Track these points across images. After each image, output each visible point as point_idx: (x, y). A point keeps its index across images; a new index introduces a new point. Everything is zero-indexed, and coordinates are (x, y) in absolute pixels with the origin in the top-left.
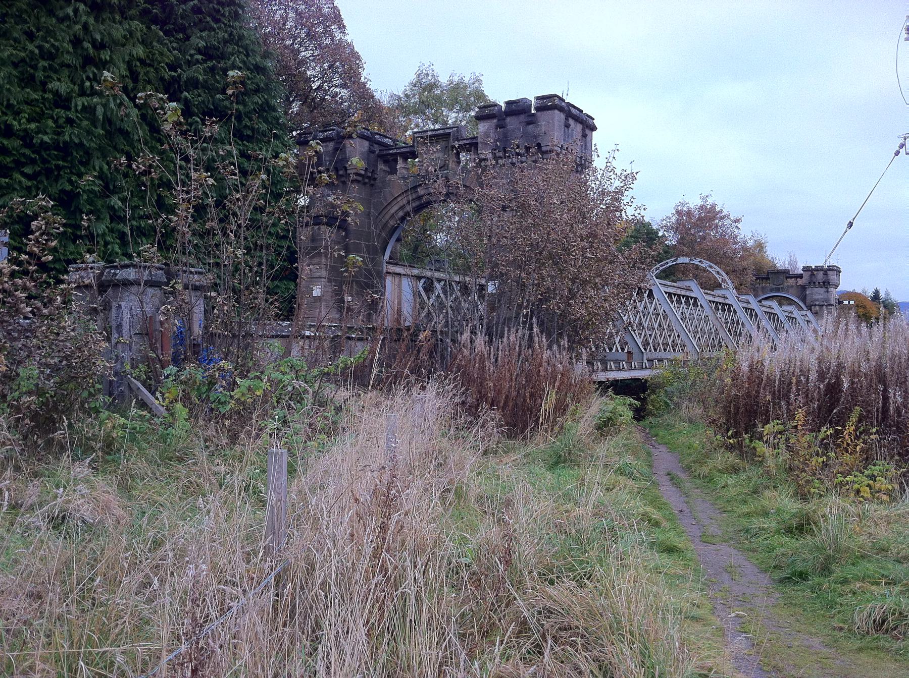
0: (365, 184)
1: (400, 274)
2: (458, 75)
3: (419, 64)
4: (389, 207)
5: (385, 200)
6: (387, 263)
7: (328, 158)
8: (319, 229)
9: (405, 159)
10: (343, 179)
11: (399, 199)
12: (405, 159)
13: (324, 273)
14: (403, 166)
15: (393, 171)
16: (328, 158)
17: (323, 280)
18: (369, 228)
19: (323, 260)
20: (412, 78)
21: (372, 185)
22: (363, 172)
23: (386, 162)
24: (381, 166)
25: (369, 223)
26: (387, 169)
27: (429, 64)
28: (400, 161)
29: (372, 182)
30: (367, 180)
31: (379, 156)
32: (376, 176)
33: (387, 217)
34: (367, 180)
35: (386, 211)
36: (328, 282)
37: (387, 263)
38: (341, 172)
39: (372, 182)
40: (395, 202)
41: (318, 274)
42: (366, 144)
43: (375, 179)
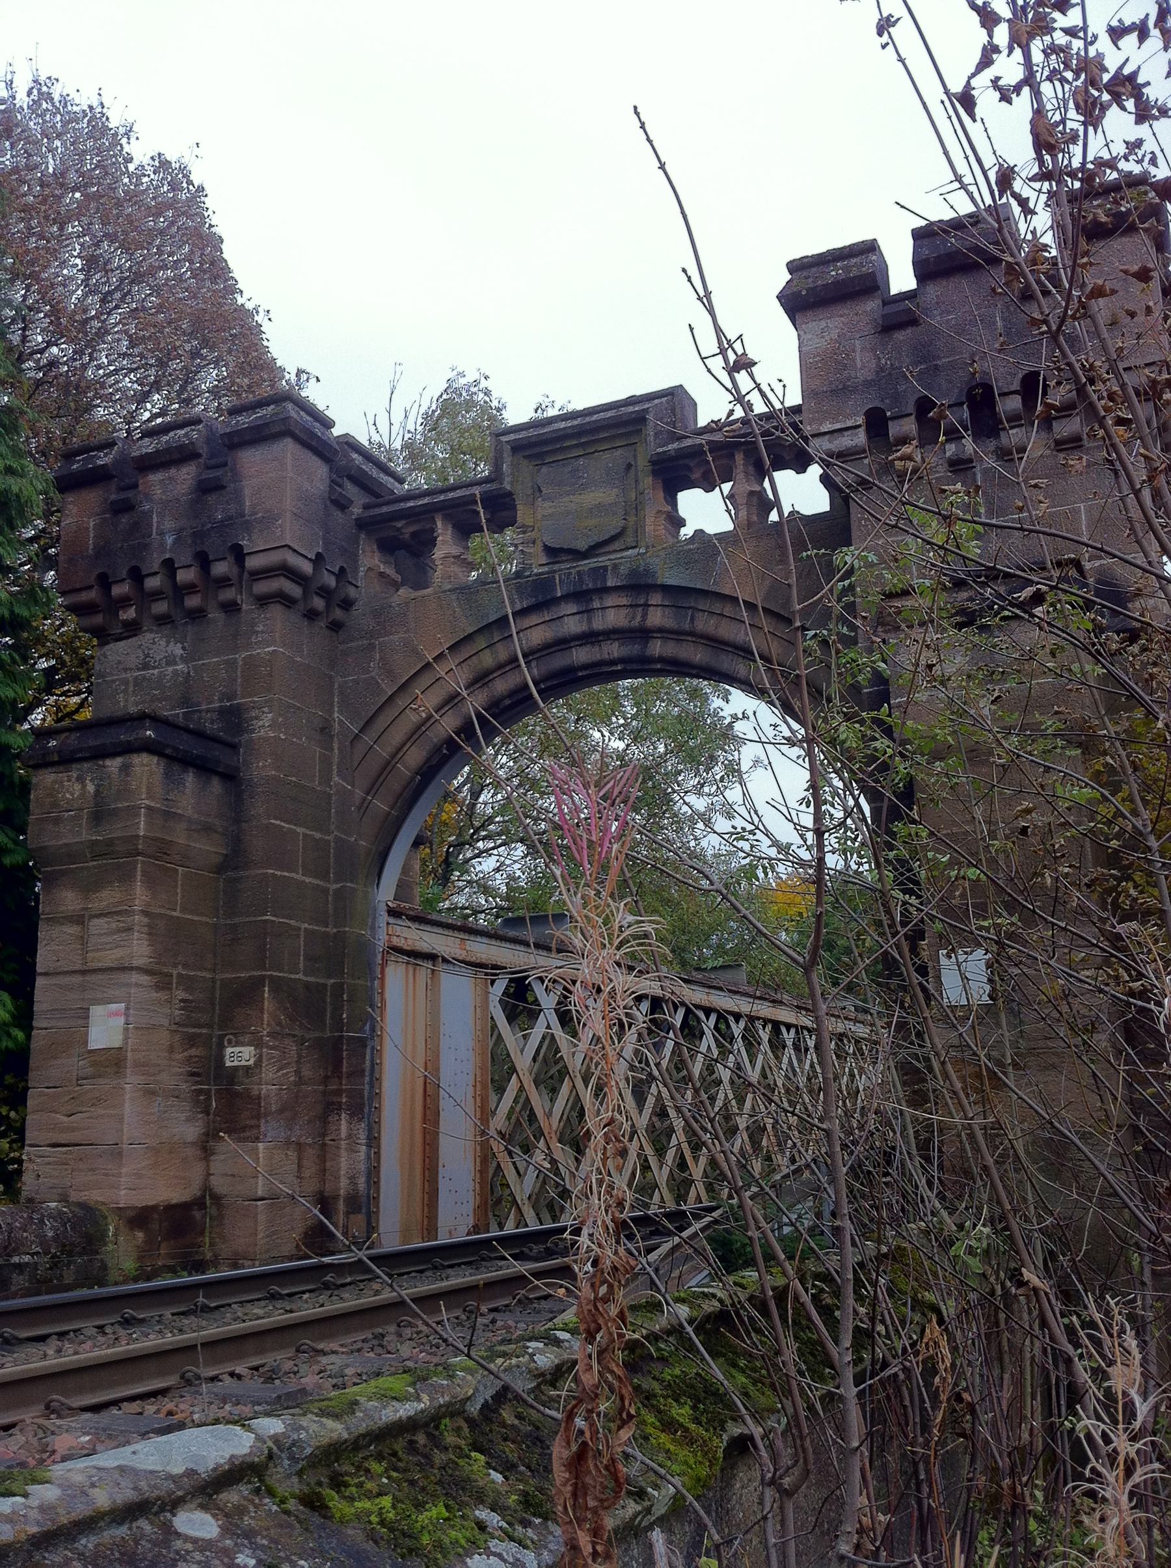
0: (311, 615)
1: (432, 957)
2: (557, 406)
3: (451, 375)
4: (401, 703)
5: (390, 673)
6: (392, 913)
7: (169, 524)
8: (125, 769)
9: (466, 529)
10: (228, 594)
11: (441, 670)
12: (466, 529)
13: (139, 950)
14: (455, 550)
15: (418, 577)
16: (169, 524)
17: (135, 977)
18: (326, 779)
19: (140, 895)
20: (437, 388)
21: (336, 626)
22: (307, 568)
23: (388, 547)
24: (370, 559)
25: (326, 762)
26: (390, 571)
27: (476, 376)
28: (444, 535)
29: (338, 614)
30: (318, 603)
31: (362, 525)
32: (352, 592)
33: (397, 736)
34: (318, 603)
35: (391, 713)
36: (158, 987)
37: (392, 913)
38: (220, 568)
39: (338, 614)
40: (426, 680)
41: (110, 957)
42: (321, 470)
43: (347, 604)
